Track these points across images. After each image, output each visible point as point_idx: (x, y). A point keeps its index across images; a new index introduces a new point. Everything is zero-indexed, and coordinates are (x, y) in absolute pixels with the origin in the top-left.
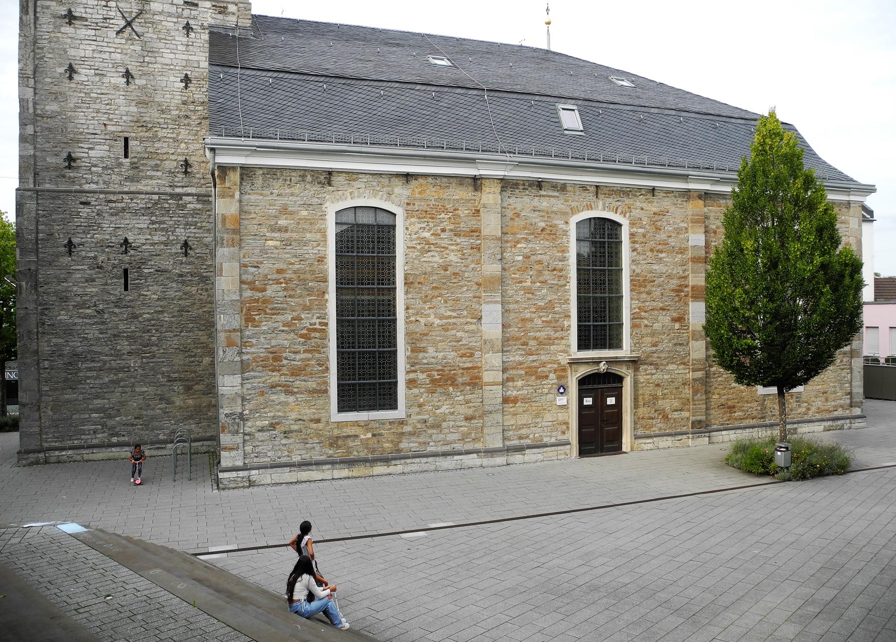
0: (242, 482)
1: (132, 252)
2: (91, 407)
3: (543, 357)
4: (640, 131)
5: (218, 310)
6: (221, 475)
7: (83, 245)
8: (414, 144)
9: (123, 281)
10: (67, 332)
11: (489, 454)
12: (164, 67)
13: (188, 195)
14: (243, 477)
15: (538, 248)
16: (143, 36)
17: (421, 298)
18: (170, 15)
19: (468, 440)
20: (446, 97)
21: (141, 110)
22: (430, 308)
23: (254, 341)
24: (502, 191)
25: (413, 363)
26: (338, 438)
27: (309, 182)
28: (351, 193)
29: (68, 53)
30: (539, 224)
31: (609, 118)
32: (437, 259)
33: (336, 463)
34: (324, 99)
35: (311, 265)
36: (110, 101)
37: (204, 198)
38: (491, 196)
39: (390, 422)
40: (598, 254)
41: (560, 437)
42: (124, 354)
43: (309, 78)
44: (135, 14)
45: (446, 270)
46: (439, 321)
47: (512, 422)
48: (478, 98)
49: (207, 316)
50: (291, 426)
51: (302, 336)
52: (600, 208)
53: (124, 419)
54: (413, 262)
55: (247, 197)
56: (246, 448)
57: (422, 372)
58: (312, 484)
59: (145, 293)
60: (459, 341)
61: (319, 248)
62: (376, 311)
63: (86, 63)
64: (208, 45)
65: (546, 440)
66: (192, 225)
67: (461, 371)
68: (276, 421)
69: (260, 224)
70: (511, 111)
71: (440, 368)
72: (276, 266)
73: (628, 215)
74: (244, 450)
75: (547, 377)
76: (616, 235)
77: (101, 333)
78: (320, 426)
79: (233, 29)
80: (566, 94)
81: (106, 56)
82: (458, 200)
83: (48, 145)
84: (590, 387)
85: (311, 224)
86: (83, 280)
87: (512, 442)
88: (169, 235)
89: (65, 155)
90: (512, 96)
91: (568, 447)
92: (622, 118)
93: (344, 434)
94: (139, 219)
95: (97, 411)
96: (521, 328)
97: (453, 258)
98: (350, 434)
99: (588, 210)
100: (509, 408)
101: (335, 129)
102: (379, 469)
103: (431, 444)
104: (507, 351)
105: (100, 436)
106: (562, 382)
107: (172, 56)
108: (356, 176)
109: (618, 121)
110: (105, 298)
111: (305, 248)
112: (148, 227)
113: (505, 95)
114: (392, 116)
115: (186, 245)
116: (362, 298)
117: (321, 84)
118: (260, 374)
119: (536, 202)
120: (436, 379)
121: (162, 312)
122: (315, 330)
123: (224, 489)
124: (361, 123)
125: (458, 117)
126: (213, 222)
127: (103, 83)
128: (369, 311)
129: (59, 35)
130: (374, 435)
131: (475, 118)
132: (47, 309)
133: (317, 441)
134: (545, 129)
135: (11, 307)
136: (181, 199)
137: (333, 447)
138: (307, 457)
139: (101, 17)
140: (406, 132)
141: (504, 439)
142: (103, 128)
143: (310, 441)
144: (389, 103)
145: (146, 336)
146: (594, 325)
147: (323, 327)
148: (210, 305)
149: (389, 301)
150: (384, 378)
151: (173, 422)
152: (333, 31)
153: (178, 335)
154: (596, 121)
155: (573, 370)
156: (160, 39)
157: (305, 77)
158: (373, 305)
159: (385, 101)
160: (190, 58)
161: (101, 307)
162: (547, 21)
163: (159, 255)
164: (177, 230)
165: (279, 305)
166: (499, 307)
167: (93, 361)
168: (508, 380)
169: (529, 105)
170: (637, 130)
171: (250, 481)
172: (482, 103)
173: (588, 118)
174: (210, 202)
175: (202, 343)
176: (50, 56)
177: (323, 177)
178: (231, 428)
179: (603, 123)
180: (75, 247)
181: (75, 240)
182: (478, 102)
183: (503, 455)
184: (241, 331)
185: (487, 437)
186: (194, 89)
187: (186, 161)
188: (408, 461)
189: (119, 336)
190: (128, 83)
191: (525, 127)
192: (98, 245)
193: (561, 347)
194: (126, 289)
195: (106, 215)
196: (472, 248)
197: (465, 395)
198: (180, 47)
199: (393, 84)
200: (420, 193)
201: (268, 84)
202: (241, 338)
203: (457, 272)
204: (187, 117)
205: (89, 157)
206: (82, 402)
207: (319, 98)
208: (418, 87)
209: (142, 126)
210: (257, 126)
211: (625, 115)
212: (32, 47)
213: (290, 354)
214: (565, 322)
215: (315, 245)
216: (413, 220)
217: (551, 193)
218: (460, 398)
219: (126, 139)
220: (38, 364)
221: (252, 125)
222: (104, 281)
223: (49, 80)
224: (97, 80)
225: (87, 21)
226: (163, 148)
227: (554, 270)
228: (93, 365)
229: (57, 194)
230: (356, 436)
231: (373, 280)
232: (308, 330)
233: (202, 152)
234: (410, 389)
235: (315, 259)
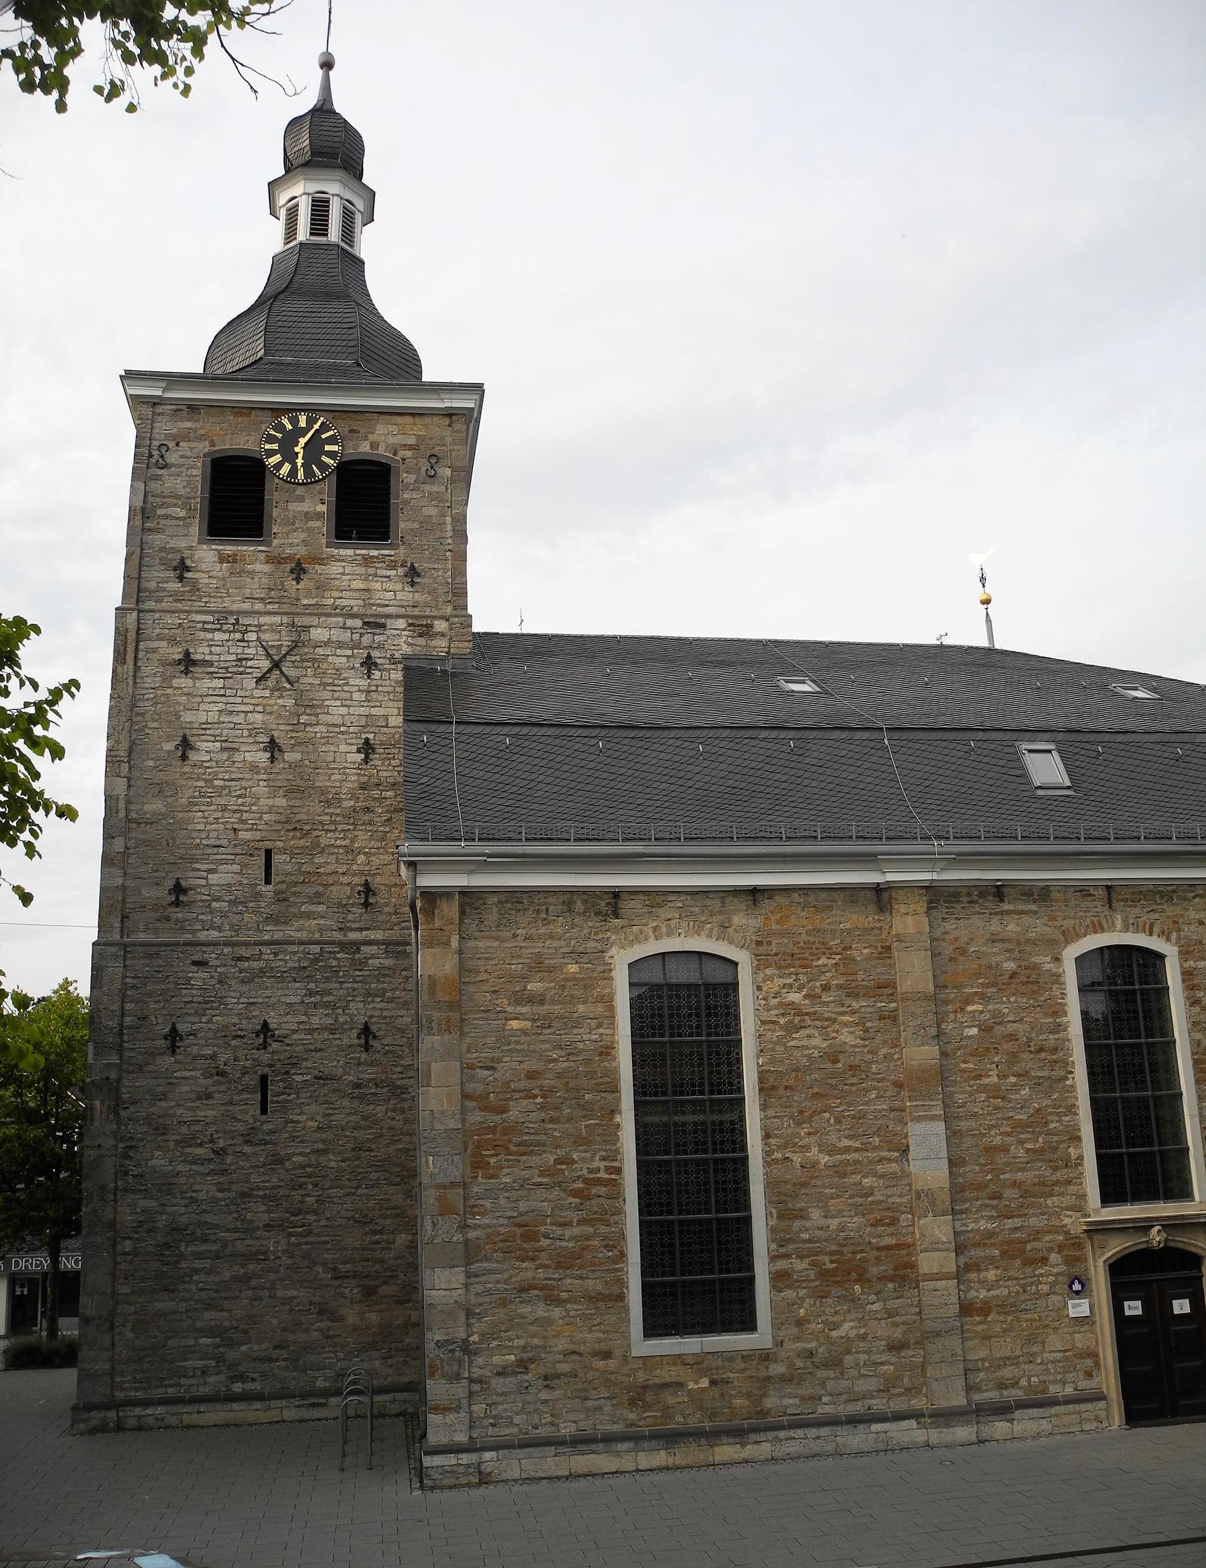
0: (465, 1474)
1: (275, 1045)
2: (198, 1324)
3: (1033, 1221)
4: (1181, 777)
5: (423, 1148)
6: (428, 1461)
7: (195, 1035)
8: (763, 834)
9: (258, 1096)
10: (164, 1188)
11: (941, 1420)
12: (332, 729)
13: (370, 943)
14: (468, 1466)
15: (1006, 1011)
16: (297, 682)
17: (792, 1117)
18: (341, 645)
19: (897, 1391)
20: (816, 747)
21: (292, 803)
22: (809, 1134)
23: (488, 1204)
24: (929, 908)
25: (781, 1240)
26: (645, 1388)
27: (579, 913)
28: (655, 929)
29: (182, 719)
30: (1005, 965)
31: (1118, 759)
32: (817, 1041)
33: (644, 1438)
34: (600, 766)
35: (588, 1062)
36: (243, 791)
37: (397, 949)
38: (909, 919)
39: (743, 1357)
40: (1124, 1015)
41: (1082, 1384)
42: (258, 1228)
43: (573, 731)
44: (288, 649)
45: (836, 1061)
46: (827, 1158)
47: (982, 1353)
48: (872, 744)
49: (403, 1158)
50: (558, 1365)
51: (575, 1193)
52: (1119, 927)
53: (256, 1348)
54: (773, 1050)
55: (471, 944)
56: (475, 1408)
57: (801, 1257)
58: (598, 1481)
59: (297, 1118)
60: (868, 1195)
61: (601, 1030)
62: (710, 1144)
63: (208, 732)
64: (401, 689)
65: (1054, 1389)
66: (377, 996)
67: (876, 1253)
68: (530, 1355)
69: (495, 992)
70: (934, 763)
71: (834, 1248)
72: (524, 1066)
73: (1174, 936)
74: (471, 1412)
75: (1044, 1260)
76: (1155, 975)
77: (220, 1191)
78: (612, 1364)
79: (442, 660)
80: (1034, 724)
81: (239, 719)
82: (849, 931)
83: (145, 868)
84: (1135, 1278)
85: (585, 987)
86: (193, 1096)
87: (986, 1394)
88: (338, 1014)
89: (170, 883)
90: (933, 735)
91: (1102, 1404)
92: (1141, 757)
93: (658, 1381)
94: (288, 988)
95: (210, 1332)
96: (985, 1165)
97: (847, 1037)
98: (668, 1380)
99: (1096, 932)
100: (975, 1325)
101: (622, 818)
102: (726, 1451)
103: (824, 1399)
104: (961, 1212)
105: (212, 1380)
106: (1077, 1269)
107: (344, 711)
108: (662, 898)
109: (1137, 763)
110: (228, 1128)
111: (575, 1031)
112: (303, 1002)
113: (920, 735)
114: (722, 788)
115: (366, 1031)
116: (683, 1119)
117: (593, 741)
118: (500, 1266)
119: (995, 925)
120: (828, 1270)
121: (324, 1152)
122: (599, 1182)
123: (432, 1488)
124: (666, 805)
125: (838, 781)
126: (414, 989)
127: (234, 762)
128: (696, 1143)
129: (170, 691)
130: (713, 1383)
131: (869, 780)
132: (131, 1147)
133: (607, 1395)
134: (1000, 790)
135: (75, 1144)
136: (358, 951)
137: (637, 1407)
138: (586, 1425)
139: (233, 657)
140: (749, 815)
141: (969, 1388)
142: (232, 836)
143: (593, 1394)
144: (714, 765)
145: (297, 1195)
146: (1129, 1154)
147: (613, 1176)
148: (407, 1138)
149: (732, 1123)
150: (728, 1271)
151: (341, 1355)
152: (609, 649)
153: (353, 1194)
154: (1094, 767)
155: (1096, 1245)
156: (325, 685)
157: (565, 731)
158: (705, 1131)
159: (706, 763)
160: (373, 711)
161: (221, 1143)
162: (984, 597)
163: (320, 1050)
164: (351, 1005)
165: (533, 1137)
166: (940, 1127)
167: (206, 1241)
168: (968, 1268)
169: (966, 748)
170: (1175, 776)
171: (480, 1473)
172: (880, 753)
173: (1077, 763)
174: (407, 955)
175: (395, 1208)
176: (155, 725)
177: (603, 904)
178: (447, 1368)
179: (1107, 770)
180: (181, 1039)
181: (182, 1027)
182: (873, 751)
183: (969, 1422)
184: (465, 1186)
185: (934, 1385)
186: (379, 763)
187: (366, 884)
188: (782, 1434)
189: (250, 1196)
190: (272, 759)
191: (963, 790)
192: (219, 1034)
193: (1068, 1200)
194: (264, 1111)
195: (233, 982)
196: (881, 1018)
197: (885, 1300)
198: (356, 696)
199: (719, 733)
200: (779, 922)
201: (503, 747)
202: (465, 1199)
203: (856, 1062)
204: (368, 810)
205: (208, 885)
206: (184, 1317)
207: (592, 765)
208: (764, 734)
209: (295, 829)
210: (487, 819)
211: (1146, 751)
212: (129, 714)
213: (554, 1228)
214: (1071, 1150)
215: (594, 1026)
216: (769, 971)
217: (1021, 907)
218: (876, 1307)
219: (268, 853)
220: (114, 1245)
221: (478, 818)
222: (227, 1098)
223: (151, 763)
224: (225, 758)
225: (212, 666)
226: (328, 863)
227: (1041, 1050)
228: (204, 1247)
229: (156, 949)
230: (680, 1385)
231: (701, 1085)
232: (586, 1181)
233: (393, 868)
234: (780, 1291)
235: (596, 1049)
